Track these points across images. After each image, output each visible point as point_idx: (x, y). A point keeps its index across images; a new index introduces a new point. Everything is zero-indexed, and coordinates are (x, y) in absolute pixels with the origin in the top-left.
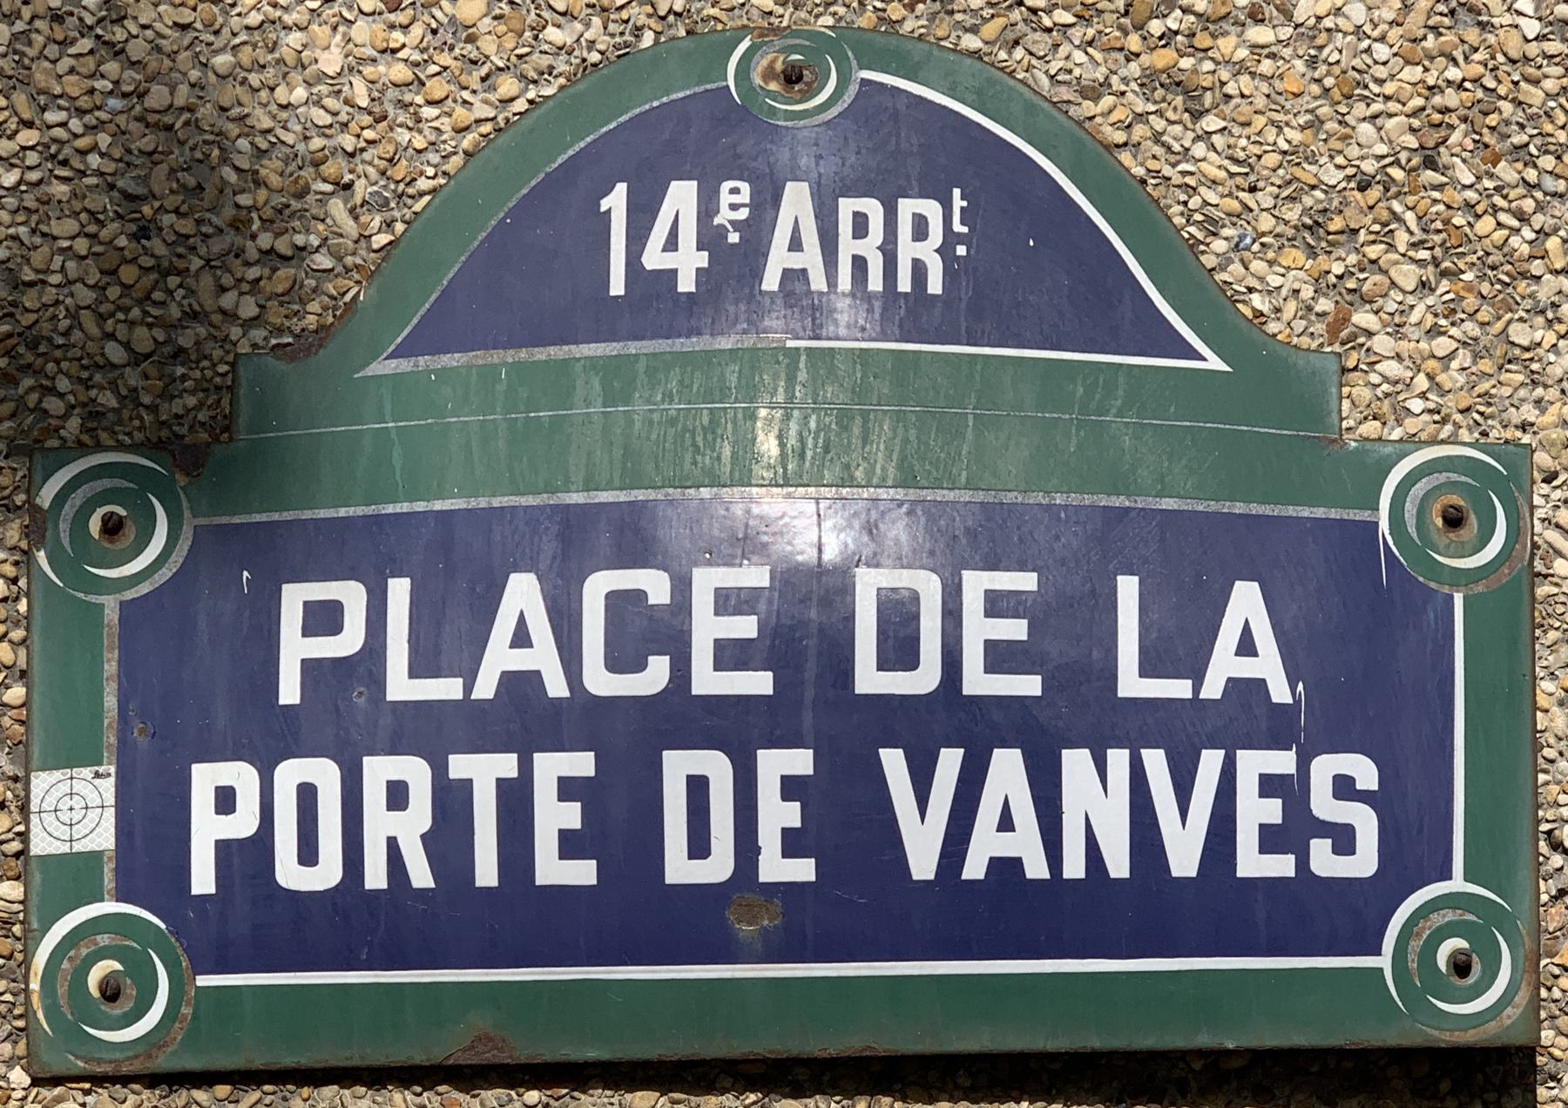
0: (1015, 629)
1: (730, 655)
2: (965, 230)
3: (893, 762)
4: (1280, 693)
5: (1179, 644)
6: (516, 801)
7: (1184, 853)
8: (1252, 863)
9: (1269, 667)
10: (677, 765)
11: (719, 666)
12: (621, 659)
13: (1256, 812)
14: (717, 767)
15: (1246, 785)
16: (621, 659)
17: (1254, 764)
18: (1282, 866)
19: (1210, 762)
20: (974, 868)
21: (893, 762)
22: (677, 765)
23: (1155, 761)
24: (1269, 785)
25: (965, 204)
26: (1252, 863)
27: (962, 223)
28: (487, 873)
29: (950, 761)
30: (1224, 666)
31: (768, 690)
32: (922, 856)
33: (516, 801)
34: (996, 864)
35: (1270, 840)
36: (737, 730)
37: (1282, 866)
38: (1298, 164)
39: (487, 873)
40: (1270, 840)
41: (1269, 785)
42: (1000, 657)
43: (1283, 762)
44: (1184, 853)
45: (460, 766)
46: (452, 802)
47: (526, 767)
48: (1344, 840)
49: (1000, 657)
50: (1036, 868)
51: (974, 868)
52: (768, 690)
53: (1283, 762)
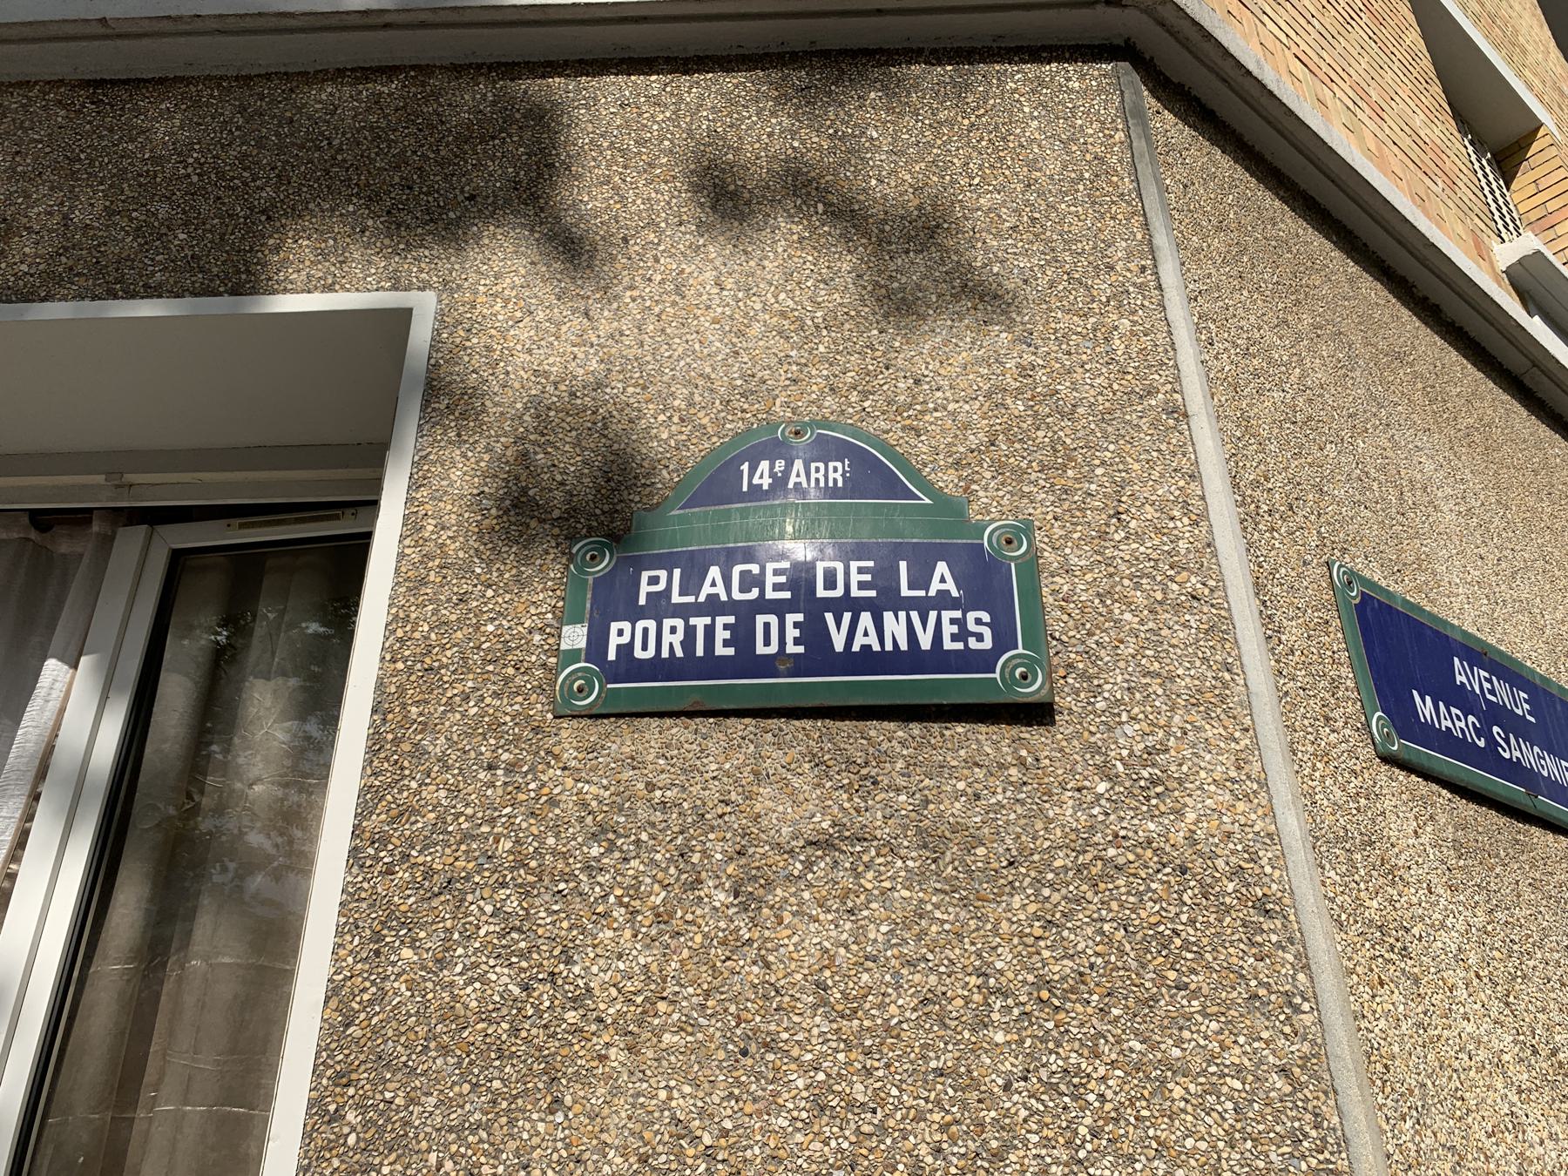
3: (829, 617)
6: (710, 631)
7: (925, 642)
10: (761, 620)
13: (948, 630)
14: (773, 619)
17: (947, 615)
18: (959, 646)
19: (933, 615)
20: (856, 648)
21: (829, 617)
22: (761, 620)
23: (914, 615)
26: (948, 645)
28: (700, 652)
29: (847, 616)
32: (839, 644)
33: (710, 631)
35: (954, 638)
36: (779, 609)
37: (959, 646)
39: (700, 652)
40: (954, 638)
42: (862, 586)
43: (958, 614)
44: (925, 642)
45: (693, 621)
50: (876, 648)
51: (856, 648)
53: (958, 614)
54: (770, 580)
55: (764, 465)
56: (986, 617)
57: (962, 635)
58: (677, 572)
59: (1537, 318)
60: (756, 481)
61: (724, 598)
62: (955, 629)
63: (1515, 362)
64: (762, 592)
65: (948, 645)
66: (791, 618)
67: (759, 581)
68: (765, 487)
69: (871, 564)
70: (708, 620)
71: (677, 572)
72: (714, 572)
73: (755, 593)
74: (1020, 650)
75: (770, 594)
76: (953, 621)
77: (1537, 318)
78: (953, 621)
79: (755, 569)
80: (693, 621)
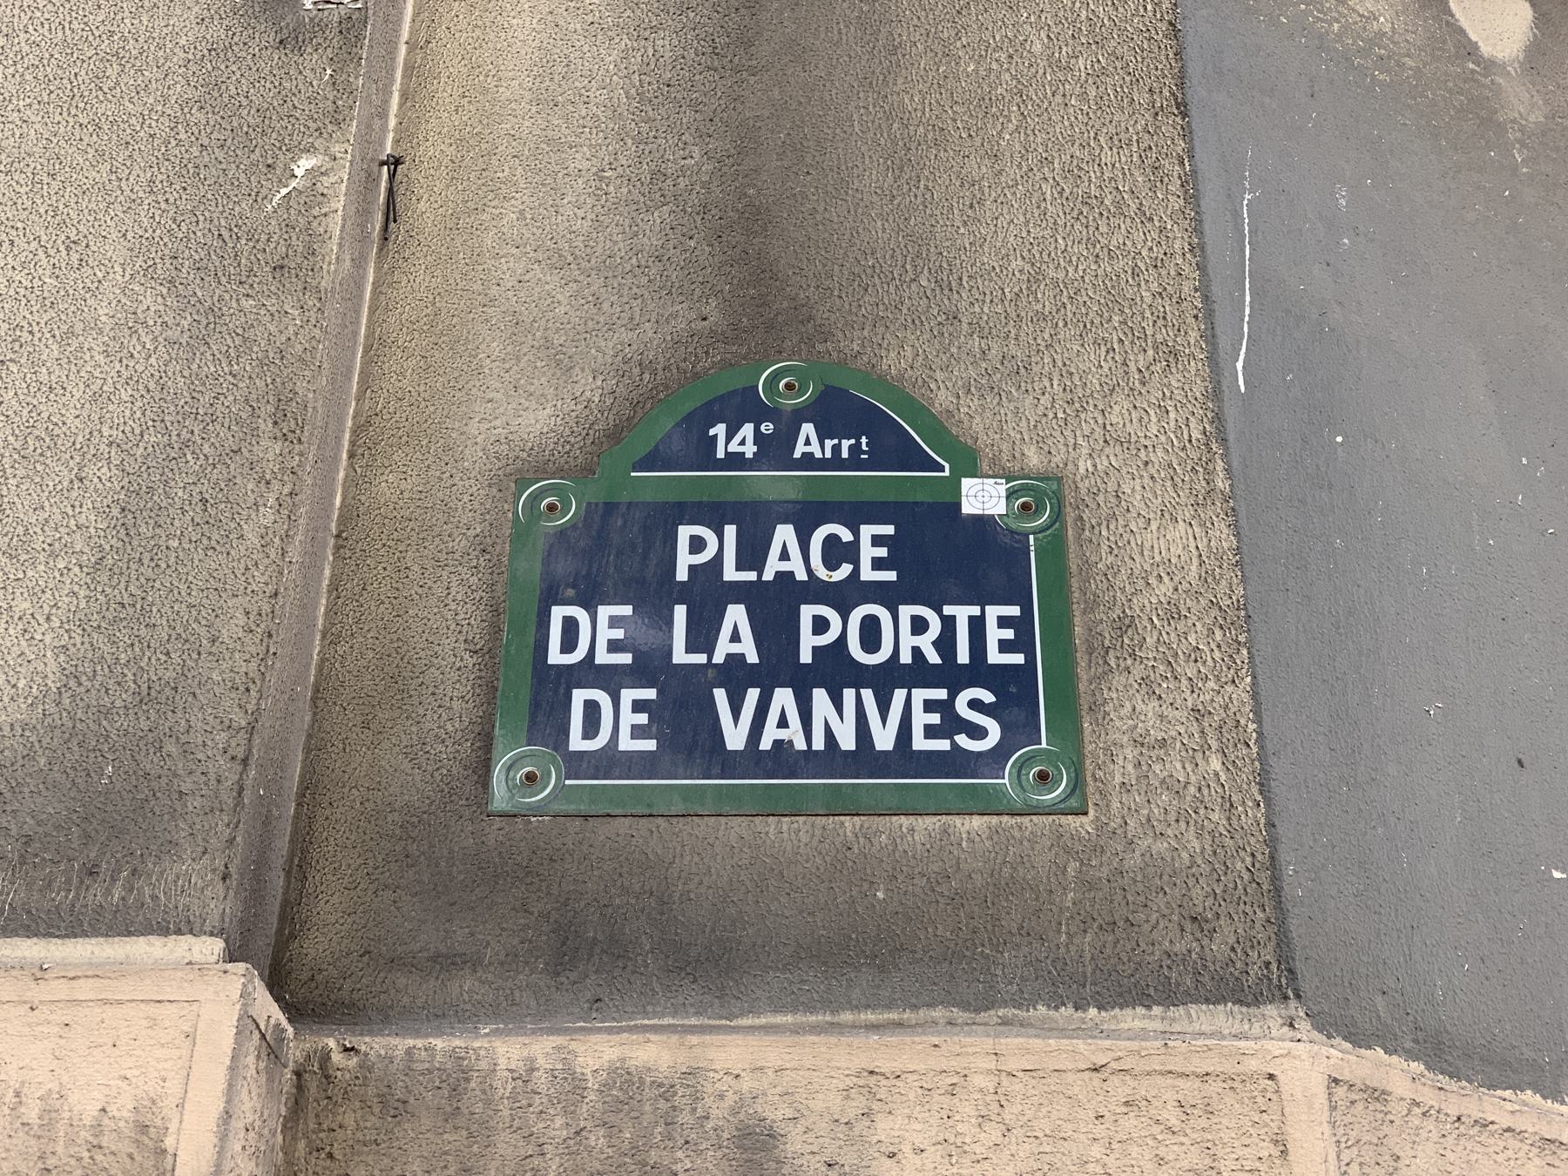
1: (878, 564)
3: (720, 695)
5: (702, 637)
6: (977, 625)
7: (884, 739)
10: (579, 696)
12: (831, 563)
13: (920, 719)
15: (917, 706)
16: (831, 563)
17: (920, 695)
18: (943, 745)
19: (899, 695)
20: (766, 744)
21: (720, 695)
22: (579, 696)
23: (868, 695)
26: (920, 743)
28: (963, 657)
29: (753, 695)
33: (977, 625)
36: (611, 679)
37: (943, 745)
39: (963, 657)
42: (614, 646)
43: (941, 694)
44: (884, 739)
45: (948, 610)
46: (949, 623)
47: (983, 611)
48: (978, 732)
50: (800, 744)
51: (766, 744)
53: (941, 694)
54: (868, 552)
56: (988, 697)
57: (951, 724)
58: (730, 531)
65: (920, 743)
66: (628, 696)
67: (850, 553)
69: (889, 530)
70: (975, 610)
71: (730, 531)
72: (785, 534)
74: (1044, 745)
76: (929, 706)
78: (929, 706)
79: (846, 535)
80: (948, 610)
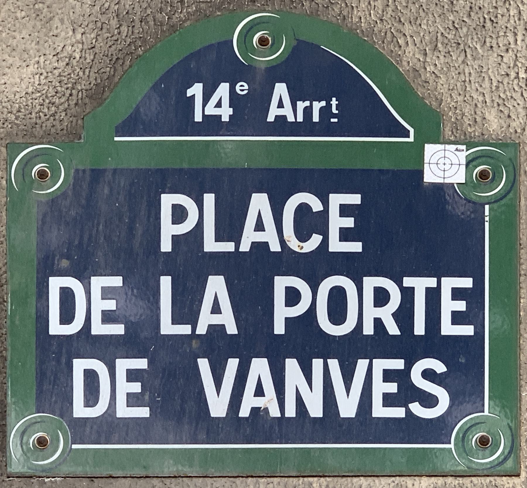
0: (111, 305)
2: (337, 112)
4: (232, 329)
8: (379, 411)
9: (228, 320)
10: (80, 366)
11: (454, 323)
13: (381, 388)
14: (98, 366)
17: (381, 365)
18: (399, 412)
19: (362, 365)
20: (244, 412)
22: (80, 366)
23: (334, 364)
24: (389, 376)
25: (337, 102)
26: (379, 411)
27: (337, 110)
30: (206, 320)
31: (122, 332)
32: (218, 406)
34: (255, 411)
35: (389, 400)
37: (399, 412)
38: (25, 115)
40: (389, 400)
41: (389, 376)
43: (398, 364)
49: (108, 317)
50: (275, 412)
51: (244, 412)
52: (122, 332)
53: (398, 364)
54: (337, 222)
55: (223, 90)
56: (440, 367)
59: (232, 109)
60: (211, 110)
61: (275, 247)
62: (392, 388)
63: (283, 412)
64: (325, 242)
68: (225, 118)
73: (316, 240)
75: (336, 245)
77: (232, 109)
